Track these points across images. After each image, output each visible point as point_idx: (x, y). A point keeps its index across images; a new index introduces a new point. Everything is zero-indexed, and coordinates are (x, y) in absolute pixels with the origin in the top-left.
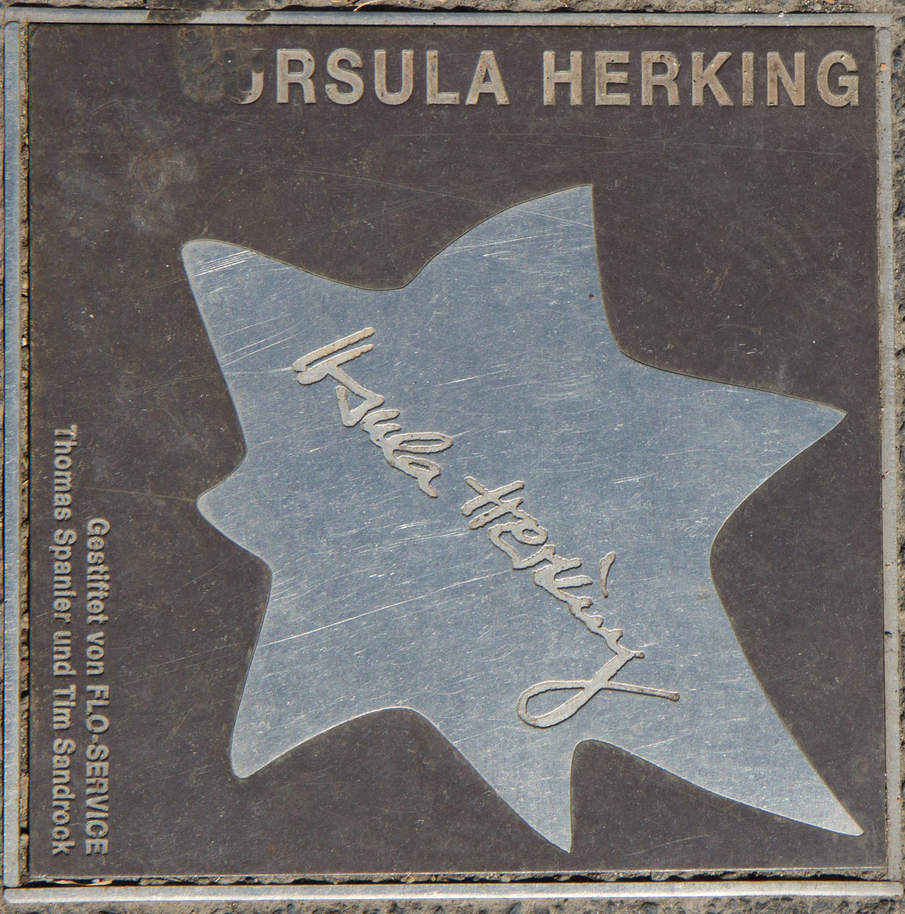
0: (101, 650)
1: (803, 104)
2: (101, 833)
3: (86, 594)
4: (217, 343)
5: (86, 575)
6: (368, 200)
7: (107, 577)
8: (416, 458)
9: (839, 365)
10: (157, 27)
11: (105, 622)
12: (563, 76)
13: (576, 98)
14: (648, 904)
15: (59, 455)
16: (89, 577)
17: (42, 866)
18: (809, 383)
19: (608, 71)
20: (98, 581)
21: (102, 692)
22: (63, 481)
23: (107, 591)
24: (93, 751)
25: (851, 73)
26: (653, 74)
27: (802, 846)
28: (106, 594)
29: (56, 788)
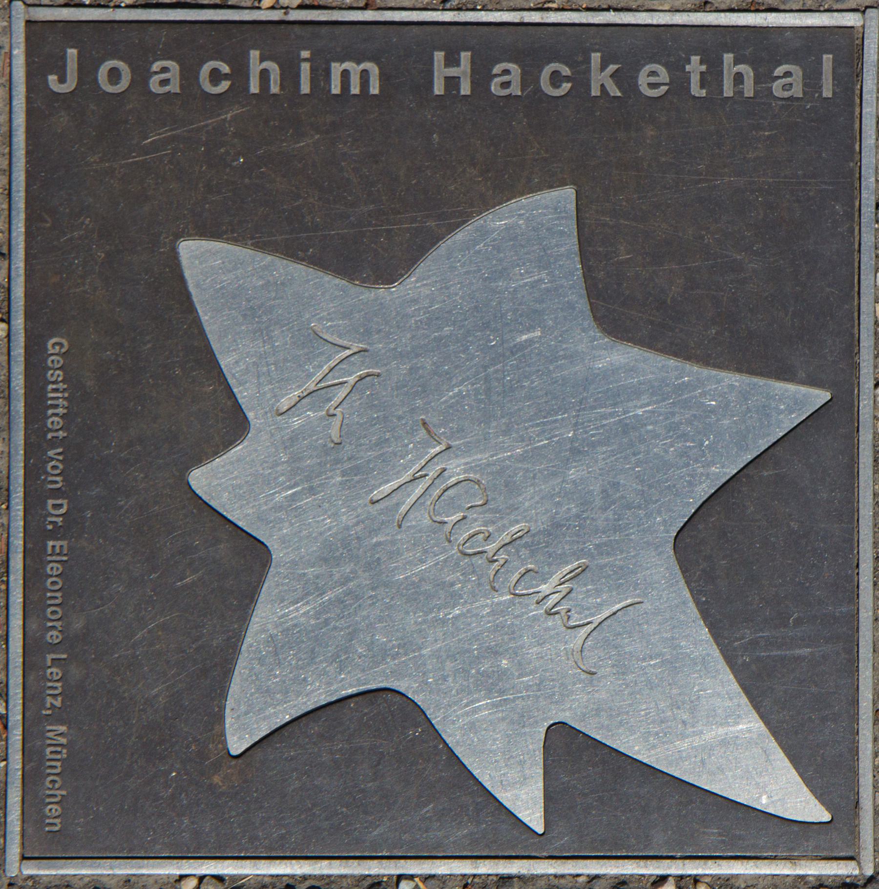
0: (61, 466)
2: (57, 786)
5: (47, 392)
6: (366, 177)
11: (64, 437)
12: (453, 72)
13: (465, 89)
14: (505, 879)
15: (49, 774)
19: (445, 67)
20: (58, 398)
21: (61, 546)
24: (52, 375)
28: (65, 411)
29: (49, 610)
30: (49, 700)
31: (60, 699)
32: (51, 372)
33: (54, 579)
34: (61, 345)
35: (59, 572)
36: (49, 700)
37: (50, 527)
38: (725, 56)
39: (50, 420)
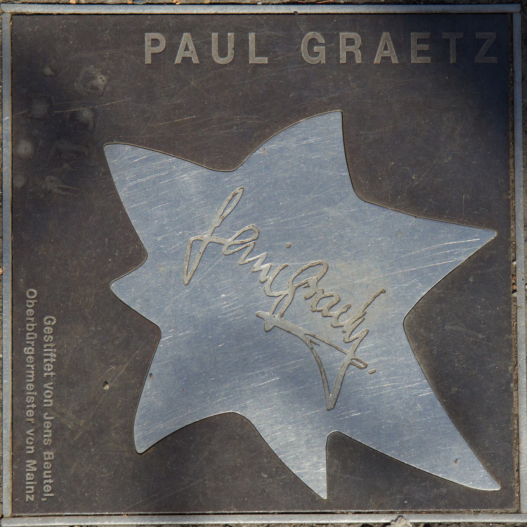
1: (345, 62)
3: (43, 374)
4: (130, 214)
7: (55, 350)
8: (304, 286)
9: (500, 218)
10: (236, 16)
13: (358, 60)
16: (45, 350)
17: (20, 508)
18: (489, 225)
22: (30, 376)
23: (55, 358)
25: (322, 44)
26: (346, 45)
27: (476, 501)
30: (28, 497)
31: (33, 496)
32: (46, 336)
33: (47, 392)
34: (52, 320)
35: (51, 332)
36: (28, 497)
37: (45, 499)
38: (267, 58)
39: (46, 328)
